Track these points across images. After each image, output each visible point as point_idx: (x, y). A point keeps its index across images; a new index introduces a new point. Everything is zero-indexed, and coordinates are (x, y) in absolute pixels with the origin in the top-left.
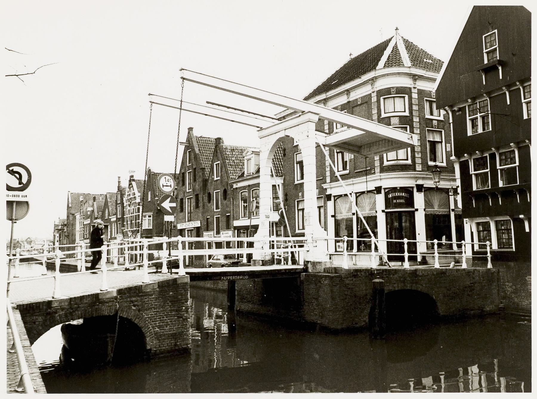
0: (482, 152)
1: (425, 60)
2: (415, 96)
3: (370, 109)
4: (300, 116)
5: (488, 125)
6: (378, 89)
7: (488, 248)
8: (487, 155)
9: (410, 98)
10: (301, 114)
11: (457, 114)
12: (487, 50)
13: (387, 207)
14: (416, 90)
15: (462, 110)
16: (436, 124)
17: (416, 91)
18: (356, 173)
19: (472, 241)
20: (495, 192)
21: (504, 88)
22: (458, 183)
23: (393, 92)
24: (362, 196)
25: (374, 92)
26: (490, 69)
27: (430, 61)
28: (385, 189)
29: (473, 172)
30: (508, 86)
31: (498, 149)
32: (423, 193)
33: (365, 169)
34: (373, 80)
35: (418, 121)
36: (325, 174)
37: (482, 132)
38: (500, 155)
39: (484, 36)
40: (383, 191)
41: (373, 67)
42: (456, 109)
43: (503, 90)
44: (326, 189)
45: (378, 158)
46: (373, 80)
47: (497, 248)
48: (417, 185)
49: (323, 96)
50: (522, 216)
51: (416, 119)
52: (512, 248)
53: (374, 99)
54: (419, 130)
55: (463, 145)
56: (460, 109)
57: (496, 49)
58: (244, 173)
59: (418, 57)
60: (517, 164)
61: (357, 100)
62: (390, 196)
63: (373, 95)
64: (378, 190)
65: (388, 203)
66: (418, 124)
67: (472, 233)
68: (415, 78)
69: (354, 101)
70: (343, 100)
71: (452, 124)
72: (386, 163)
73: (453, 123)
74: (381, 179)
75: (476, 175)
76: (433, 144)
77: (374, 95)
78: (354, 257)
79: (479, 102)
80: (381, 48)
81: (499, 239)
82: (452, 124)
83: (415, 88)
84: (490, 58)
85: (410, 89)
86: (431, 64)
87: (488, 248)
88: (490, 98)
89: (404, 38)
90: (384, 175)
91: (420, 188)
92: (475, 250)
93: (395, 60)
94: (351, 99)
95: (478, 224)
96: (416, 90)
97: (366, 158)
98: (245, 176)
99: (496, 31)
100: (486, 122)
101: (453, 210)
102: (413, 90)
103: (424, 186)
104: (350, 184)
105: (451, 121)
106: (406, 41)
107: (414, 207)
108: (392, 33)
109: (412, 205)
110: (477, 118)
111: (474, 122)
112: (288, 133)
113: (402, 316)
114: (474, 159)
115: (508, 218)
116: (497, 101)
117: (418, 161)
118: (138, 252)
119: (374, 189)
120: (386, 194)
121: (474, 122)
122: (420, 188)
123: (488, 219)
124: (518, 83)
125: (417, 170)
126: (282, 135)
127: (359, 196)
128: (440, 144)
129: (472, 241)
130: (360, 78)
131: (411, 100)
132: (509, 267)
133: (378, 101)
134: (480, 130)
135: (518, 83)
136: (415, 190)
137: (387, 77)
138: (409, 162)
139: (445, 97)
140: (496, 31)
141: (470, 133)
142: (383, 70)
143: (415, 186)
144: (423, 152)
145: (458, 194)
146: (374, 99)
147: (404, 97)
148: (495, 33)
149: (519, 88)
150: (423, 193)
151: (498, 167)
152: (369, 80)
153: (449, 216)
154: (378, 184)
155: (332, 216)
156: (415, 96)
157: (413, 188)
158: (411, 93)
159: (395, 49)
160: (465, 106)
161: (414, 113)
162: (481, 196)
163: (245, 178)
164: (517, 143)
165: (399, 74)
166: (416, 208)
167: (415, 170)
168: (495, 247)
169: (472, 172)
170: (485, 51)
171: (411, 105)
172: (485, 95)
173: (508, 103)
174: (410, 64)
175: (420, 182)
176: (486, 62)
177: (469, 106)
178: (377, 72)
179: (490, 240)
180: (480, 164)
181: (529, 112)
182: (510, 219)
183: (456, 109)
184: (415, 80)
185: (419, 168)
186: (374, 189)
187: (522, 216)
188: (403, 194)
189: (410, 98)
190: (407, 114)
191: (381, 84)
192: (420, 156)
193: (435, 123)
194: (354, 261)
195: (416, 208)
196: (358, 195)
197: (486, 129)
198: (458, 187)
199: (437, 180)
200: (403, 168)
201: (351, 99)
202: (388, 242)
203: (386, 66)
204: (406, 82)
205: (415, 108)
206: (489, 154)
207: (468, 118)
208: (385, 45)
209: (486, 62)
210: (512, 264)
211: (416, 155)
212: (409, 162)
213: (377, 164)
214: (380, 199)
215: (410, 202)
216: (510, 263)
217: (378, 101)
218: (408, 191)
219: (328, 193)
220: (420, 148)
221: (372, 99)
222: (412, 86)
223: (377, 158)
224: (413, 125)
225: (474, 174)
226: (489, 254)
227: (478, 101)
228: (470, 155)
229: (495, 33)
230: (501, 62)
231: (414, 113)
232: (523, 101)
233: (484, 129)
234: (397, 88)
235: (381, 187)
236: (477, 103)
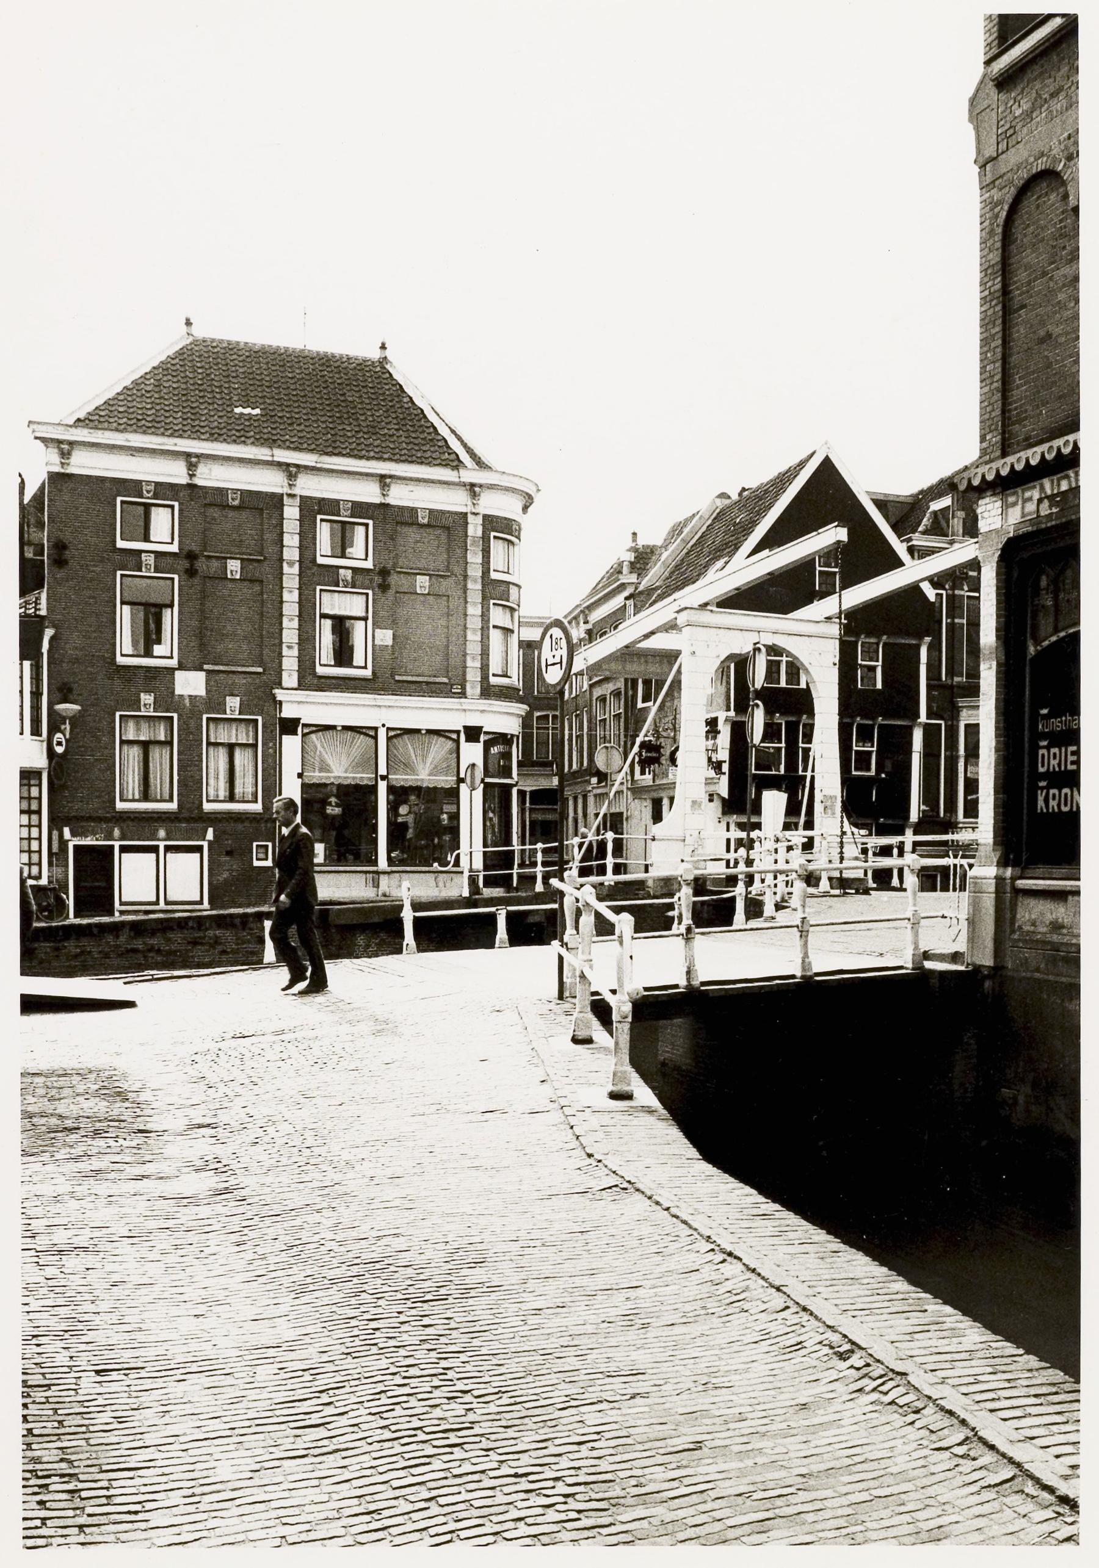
23: (148, 492)
24: (406, 737)
40: (482, 738)
76: (341, 625)
83: (476, 514)
90: (484, 704)
101: (383, 778)
102: (470, 518)
105: (988, 635)
118: (610, 861)
120: (487, 745)
127: (396, 736)
128: (169, 610)
137: (237, 464)
143: (462, 729)
153: (374, 789)
154: (473, 721)
157: (458, 732)
184: (474, 495)
193: (150, 560)
196: (391, 734)
202: (485, 853)
214: (472, 753)
217: (485, 539)
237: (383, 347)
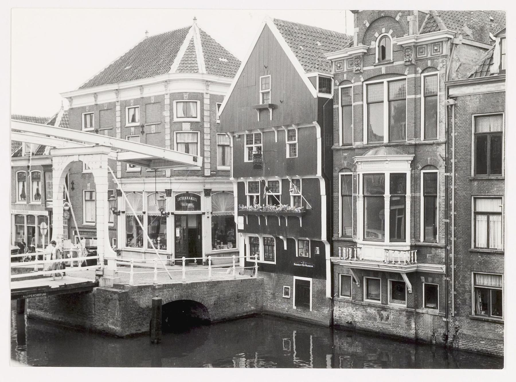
2: (207, 101)
4: (94, 146)
9: (202, 104)
10: (94, 145)
14: (209, 95)
27: (226, 60)
32: (210, 197)
35: (209, 126)
36: (116, 168)
51: (207, 125)
53: (167, 101)
54: (209, 135)
56: (240, 136)
58: (21, 150)
59: (214, 53)
60: (280, 193)
63: (166, 97)
64: (169, 192)
67: (245, 245)
68: (207, 83)
69: (146, 98)
77: (167, 97)
80: (177, 37)
85: (202, 94)
89: (202, 29)
91: (208, 192)
94: (145, 95)
95: (250, 238)
96: (209, 95)
98: (23, 155)
99: (270, 76)
102: (205, 96)
103: (212, 190)
106: (203, 35)
112: (81, 158)
113: (178, 324)
120: (177, 197)
122: (208, 192)
123: (257, 235)
126: (75, 159)
129: (245, 255)
132: (271, 277)
133: (171, 105)
143: (203, 190)
146: (167, 101)
147: (196, 102)
154: (168, 187)
156: (207, 101)
158: (203, 98)
163: (22, 158)
165: (193, 80)
169: (247, 193)
170: (261, 91)
171: (202, 111)
175: (208, 187)
181: (222, 255)
188: (192, 198)
189: (202, 104)
190: (198, 119)
191: (175, 88)
192: (209, 161)
203: (181, 70)
205: (206, 113)
210: (273, 275)
216: (272, 274)
217: (171, 105)
221: (165, 100)
222: (204, 92)
230: (271, 106)
231: (205, 119)
234: (190, 93)
235: (171, 190)
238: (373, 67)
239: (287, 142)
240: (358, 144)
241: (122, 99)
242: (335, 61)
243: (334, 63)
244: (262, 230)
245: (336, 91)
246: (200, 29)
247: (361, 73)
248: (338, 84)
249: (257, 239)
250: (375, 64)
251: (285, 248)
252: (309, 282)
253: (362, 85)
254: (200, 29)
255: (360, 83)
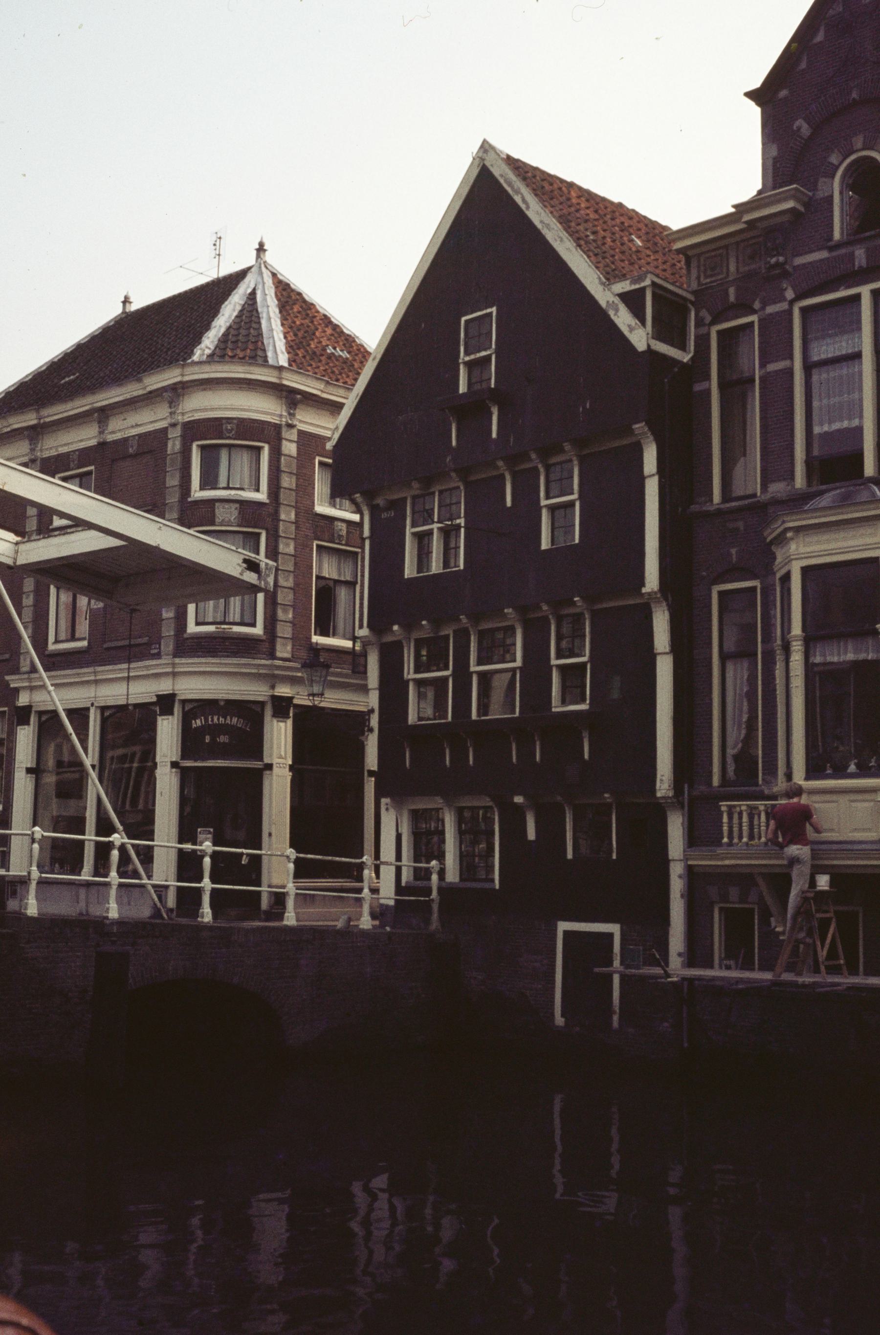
0: (437, 624)
1: (330, 350)
2: (290, 448)
3: (160, 471)
5: (457, 556)
6: (187, 418)
7: (435, 877)
8: (448, 631)
9: (276, 453)
11: (384, 515)
12: (467, 359)
13: (184, 755)
14: (295, 431)
15: (398, 506)
16: (344, 533)
17: (293, 435)
18: (108, 649)
19: (399, 857)
20: (461, 731)
21: (500, 463)
22: (373, 700)
23: (230, 431)
25: (174, 425)
26: (471, 411)
27: (345, 355)
28: (184, 702)
29: (412, 676)
30: (513, 460)
31: (476, 618)
33: (126, 642)
34: (178, 391)
35: (293, 516)
37: (415, 575)
38: (481, 635)
39: (463, 319)
40: (177, 709)
41: (180, 354)
42: (380, 501)
43: (497, 468)
44: (17, 691)
45: (171, 614)
46: (178, 391)
47: (457, 880)
48: (274, 698)
49: (29, 419)
50: (518, 799)
51: (287, 515)
52: (493, 880)
53: (174, 445)
55: (394, 600)
57: (488, 359)
60: (519, 663)
61: (125, 440)
62: (197, 723)
64: (166, 703)
65: (190, 742)
66: (293, 527)
68: (293, 399)
70: (86, 437)
71: (367, 543)
72: (192, 628)
73: (371, 537)
74: (128, 678)
75: (419, 683)
77: (175, 434)
78: (82, 892)
79: (441, 492)
81: (464, 858)
82: (367, 543)
84: (473, 381)
86: (345, 361)
87: (435, 877)
88: (467, 485)
90: (185, 664)
91: (281, 707)
92: (403, 884)
93: (245, 339)
97: (131, 613)
99: (494, 310)
100: (452, 545)
102: (285, 434)
103: (295, 701)
104: (88, 682)
107: (261, 759)
108: (250, 260)
109: (258, 754)
110: (430, 533)
111: (423, 539)
114: (416, 640)
115: (487, 802)
116: (481, 496)
117: (284, 631)
119: (154, 699)
121: (423, 539)
122: (281, 707)
123: (438, 802)
124: (533, 456)
125: (279, 654)
129: (399, 857)
130: (140, 380)
131: (279, 461)
134: (436, 567)
135: (533, 456)
136: (268, 712)
138: (258, 630)
139: (355, 465)
140: (494, 310)
141: (410, 571)
142: (207, 368)
144: (299, 607)
145: (371, 730)
146: (174, 445)
148: (491, 313)
149: (536, 469)
150: (290, 722)
151: (474, 668)
152: (164, 389)
154: (165, 687)
155: (29, 771)
156: (290, 448)
157: (262, 704)
159: (250, 312)
160: (405, 499)
161: (282, 496)
162: (423, 737)
164: (522, 610)
166: (267, 760)
167: (272, 655)
168: (452, 876)
169: (409, 673)
172: (453, 474)
173: (509, 503)
174: (283, 360)
175: (283, 690)
176: (463, 388)
177: (414, 498)
178: (188, 370)
179: (441, 857)
180: (433, 655)
182: (491, 804)
183: (380, 501)
185: (284, 650)
186: (154, 699)
187: (518, 799)
189: (276, 453)
191: (202, 405)
194: (82, 904)
195: (267, 760)
197: (452, 564)
198: (372, 711)
199: (316, 689)
200: (244, 647)
201: (110, 438)
204: (262, 408)
205: (287, 482)
206: (454, 631)
207: (409, 530)
208: (223, 287)
209: (463, 388)
211: (280, 614)
212: (258, 630)
213: (168, 631)
215: (252, 743)
218: (250, 714)
219: (23, 700)
220: (291, 596)
223: (168, 614)
224: (276, 529)
225: (414, 680)
226: (434, 894)
227: (436, 489)
228: (409, 627)
229: (491, 313)
230: (496, 396)
232: (544, 502)
233: (446, 564)
234: (241, 421)
236: (433, 493)
237: (261, 249)
238: (824, 254)
239: (554, 662)
240: (778, 488)
241: (46, 454)
242: (699, 255)
243: (694, 264)
244: (450, 786)
245: (703, 342)
246: (274, 275)
247: (785, 274)
248: (708, 319)
249: (434, 815)
250: (830, 244)
251: (509, 503)
252: (610, 936)
253: (790, 312)
254: (274, 275)
255: (784, 306)
